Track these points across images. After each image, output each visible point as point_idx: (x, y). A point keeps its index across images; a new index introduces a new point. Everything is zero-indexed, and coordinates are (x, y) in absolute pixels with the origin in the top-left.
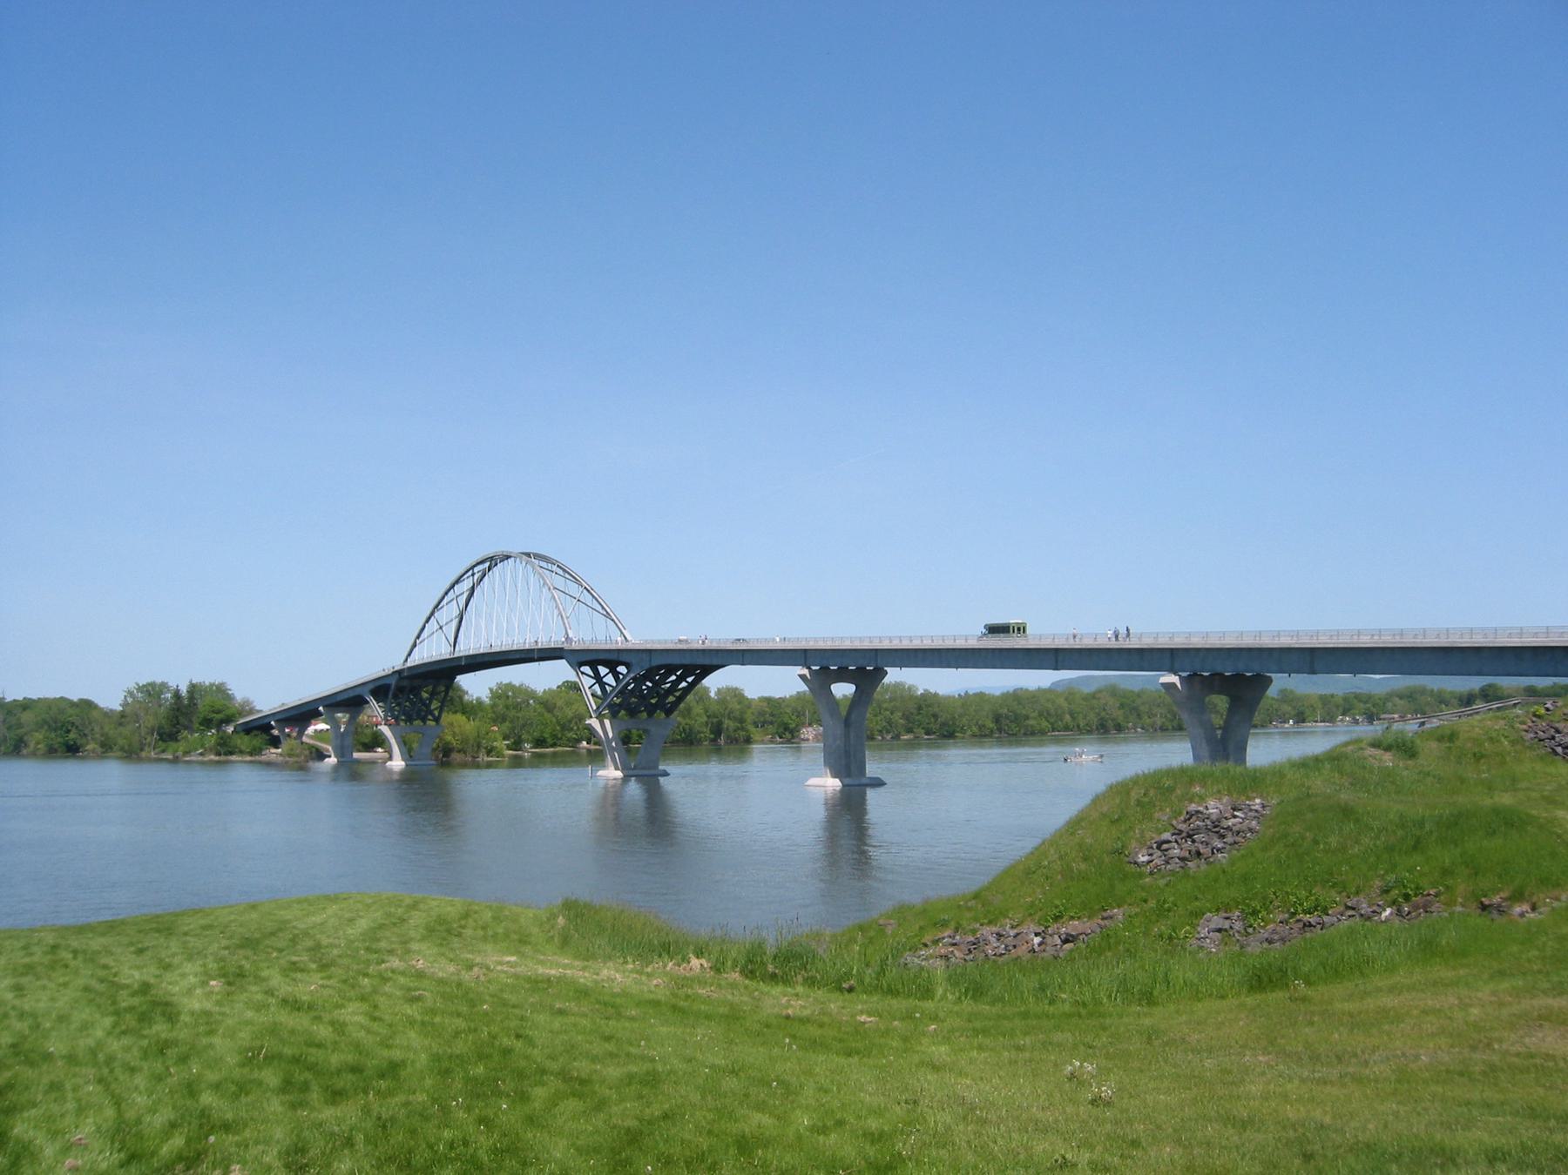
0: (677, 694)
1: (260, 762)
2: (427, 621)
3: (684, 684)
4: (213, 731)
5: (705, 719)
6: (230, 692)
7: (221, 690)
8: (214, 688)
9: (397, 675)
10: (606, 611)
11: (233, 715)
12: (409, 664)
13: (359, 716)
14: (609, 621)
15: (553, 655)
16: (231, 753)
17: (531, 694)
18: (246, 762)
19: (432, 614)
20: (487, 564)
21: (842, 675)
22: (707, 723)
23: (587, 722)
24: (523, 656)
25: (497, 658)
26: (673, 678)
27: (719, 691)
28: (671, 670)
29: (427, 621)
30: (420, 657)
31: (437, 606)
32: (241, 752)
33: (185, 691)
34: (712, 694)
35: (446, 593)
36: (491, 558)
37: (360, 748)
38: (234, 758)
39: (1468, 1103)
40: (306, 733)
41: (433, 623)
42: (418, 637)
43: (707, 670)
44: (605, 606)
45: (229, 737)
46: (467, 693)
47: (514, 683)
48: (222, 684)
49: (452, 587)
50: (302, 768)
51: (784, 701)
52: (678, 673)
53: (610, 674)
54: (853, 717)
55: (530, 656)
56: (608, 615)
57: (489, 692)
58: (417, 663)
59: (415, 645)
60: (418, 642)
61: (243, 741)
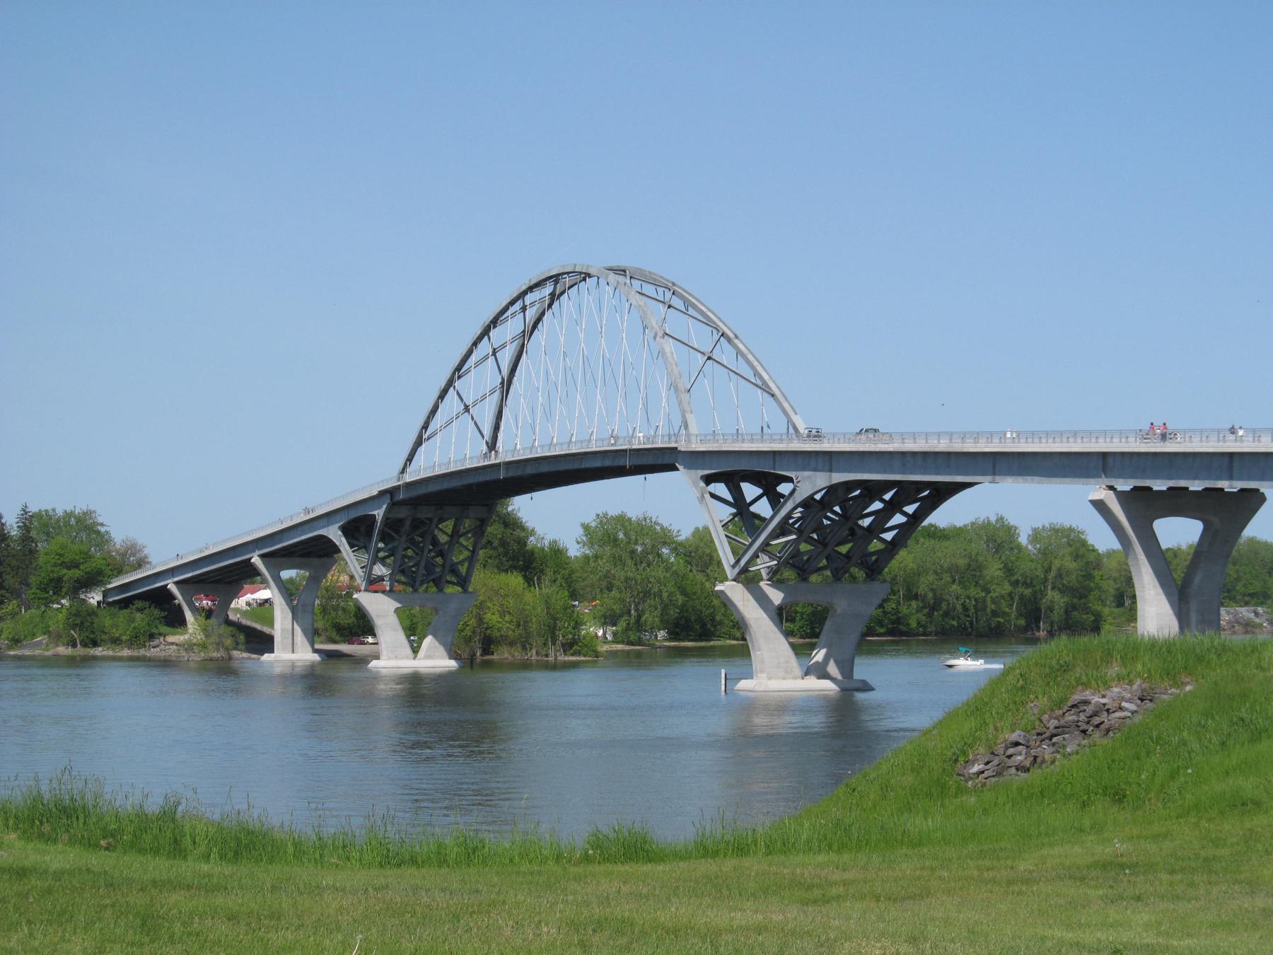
0: (888, 536)
1: (150, 659)
2: (442, 396)
3: (898, 519)
4: (63, 601)
5: (1007, 588)
6: (103, 530)
7: (85, 525)
8: (73, 521)
9: (387, 499)
10: (761, 378)
11: (100, 572)
12: (409, 477)
13: (325, 576)
14: (497, 395)
15: (660, 462)
16: (95, 644)
17: (665, 537)
18: (120, 659)
19: (450, 383)
20: (548, 289)
21: (1177, 503)
22: (1010, 594)
23: (717, 588)
24: (608, 463)
25: (563, 467)
26: (877, 505)
27: (1036, 536)
28: (872, 490)
29: (442, 396)
30: (432, 463)
31: (459, 368)
32: (116, 641)
33: (15, 526)
34: (1023, 540)
35: (475, 344)
36: (556, 278)
37: (334, 635)
38: (98, 651)
39: (532, 873)
40: (233, 606)
41: (451, 404)
42: (425, 427)
43: (942, 493)
44: (759, 368)
45: (92, 613)
46: (533, 532)
47: (629, 515)
48: (88, 514)
49: (486, 332)
50: (224, 669)
51: (1175, 555)
52: (887, 497)
53: (748, 500)
54: (1197, 579)
55: (620, 462)
56: (765, 388)
57: (581, 531)
58: (423, 475)
59: (419, 442)
60: (425, 436)
61: (119, 623)
